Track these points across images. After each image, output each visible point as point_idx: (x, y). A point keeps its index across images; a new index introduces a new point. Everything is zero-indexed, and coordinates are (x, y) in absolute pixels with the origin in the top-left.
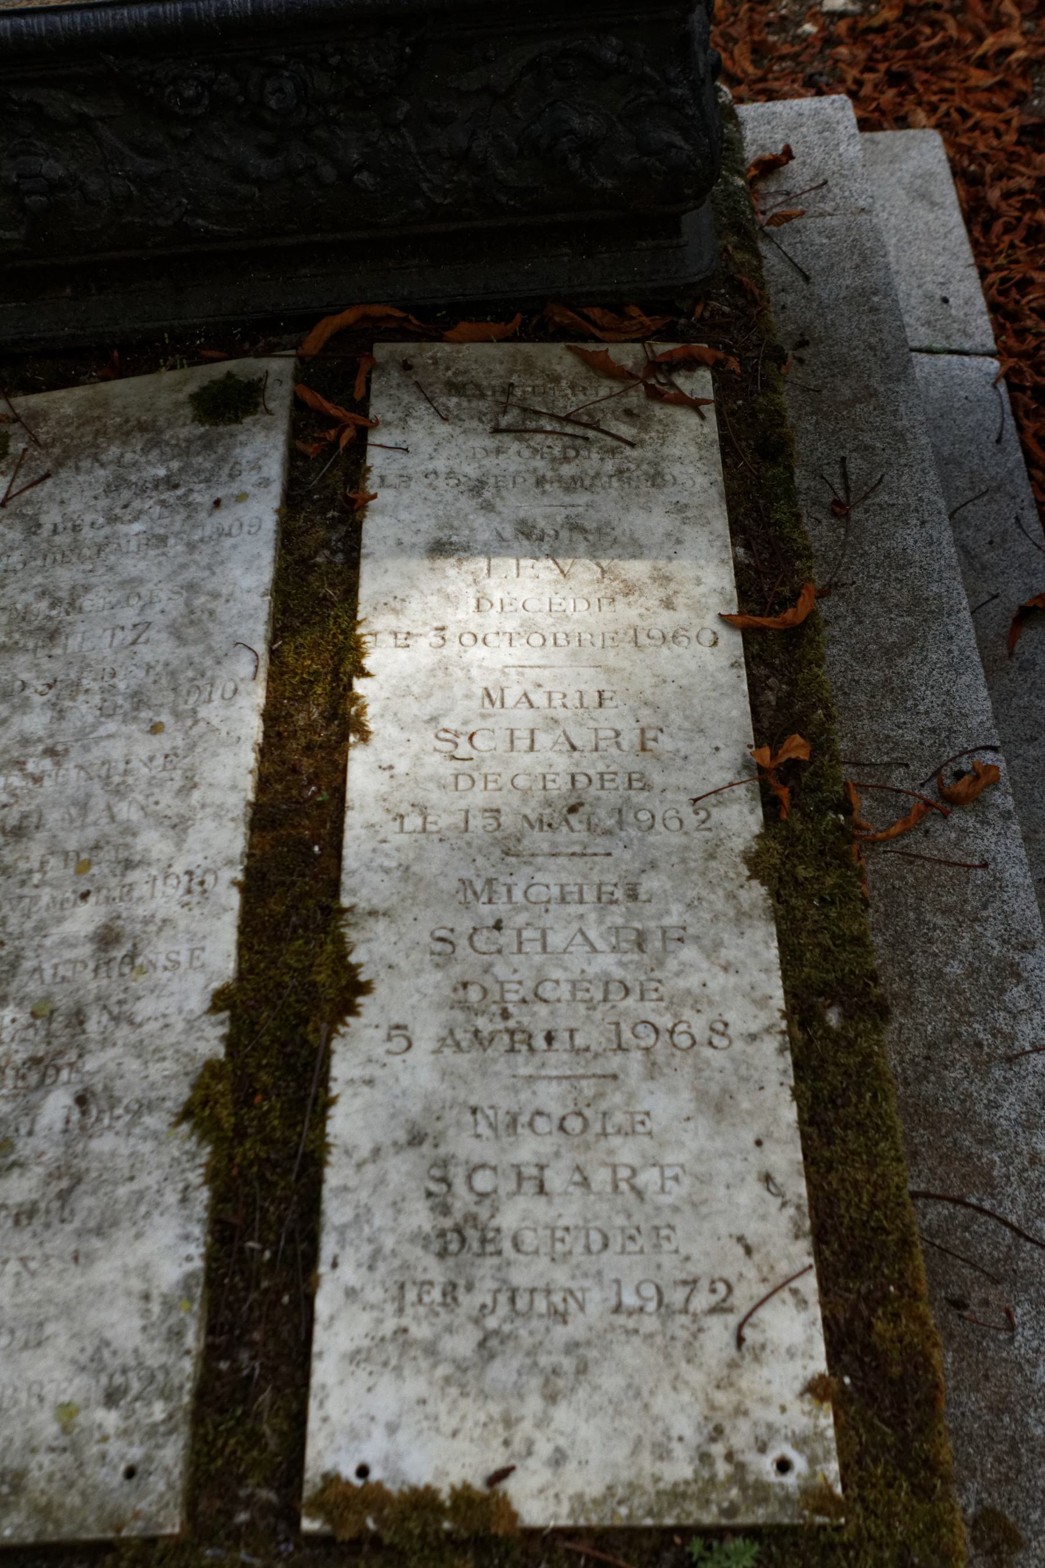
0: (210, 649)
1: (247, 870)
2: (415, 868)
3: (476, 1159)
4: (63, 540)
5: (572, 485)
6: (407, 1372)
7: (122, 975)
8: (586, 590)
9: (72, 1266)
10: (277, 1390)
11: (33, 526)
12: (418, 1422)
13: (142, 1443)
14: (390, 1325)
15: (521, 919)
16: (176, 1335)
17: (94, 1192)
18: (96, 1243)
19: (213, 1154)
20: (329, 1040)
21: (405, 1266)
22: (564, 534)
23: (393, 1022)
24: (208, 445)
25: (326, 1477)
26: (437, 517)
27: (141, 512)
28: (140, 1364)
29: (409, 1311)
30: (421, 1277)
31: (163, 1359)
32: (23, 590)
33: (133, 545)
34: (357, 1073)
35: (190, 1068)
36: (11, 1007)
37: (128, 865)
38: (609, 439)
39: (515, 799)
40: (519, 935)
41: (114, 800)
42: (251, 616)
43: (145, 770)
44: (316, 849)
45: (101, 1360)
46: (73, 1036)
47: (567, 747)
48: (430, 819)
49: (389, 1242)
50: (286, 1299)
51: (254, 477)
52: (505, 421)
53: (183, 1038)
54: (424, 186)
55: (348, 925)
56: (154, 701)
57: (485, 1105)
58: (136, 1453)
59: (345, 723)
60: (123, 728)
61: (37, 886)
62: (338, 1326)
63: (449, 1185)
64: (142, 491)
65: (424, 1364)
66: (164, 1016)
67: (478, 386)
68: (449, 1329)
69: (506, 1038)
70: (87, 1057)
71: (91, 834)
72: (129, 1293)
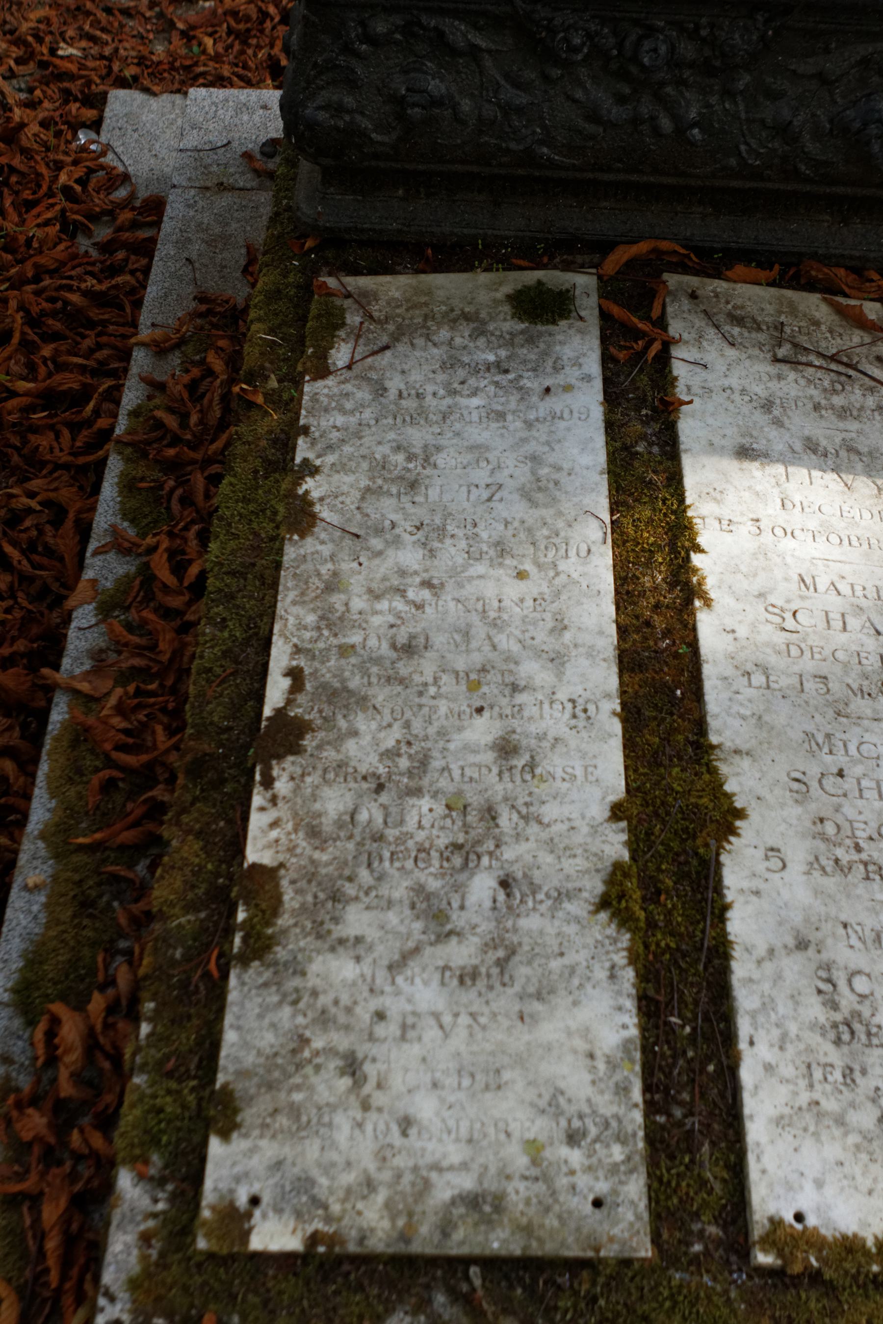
0: (560, 514)
1: (623, 705)
2: (766, 718)
3: (852, 966)
4: (409, 404)
5: (843, 413)
6: (824, 1138)
7: (524, 781)
8: (868, 503)
9: (519, 1023)
10: (713, 1144)
11: (380, 390)
12: (840, 1180)
13: (606, 1178)
14: (804, 1098)
15: (859, 770)
16: (623, 1090)
17: (529, 963)
18: (537, 1006)
19: (632, 940)
20: (718, 854)
21: (809, 1050)
22: (843, 453)
23: (769, 845)
24: (531, 340)
25: (771, 1220)
26: (738, 426)
27: (477, 389)
28: (594, 1112)
29: (818, 1087)
30: (823, 1060)
31: (614, 1109)
32: (380, 443)
33: (475, 417)
34: (745, 884)
35: (600, 866)
36: (427, 798)
37: (515, 688)
38: (867, 379)
39: (838, 669)
40: (859, 783)
41: (493, 632)
42: (593, 490)
43: (518, 610)
44: (679, 692)
45: (558, 1106)
46: (489, 829)
47: (873, 632)
48: (772, 678)
49: (793, 1028)
50: (711, 1068)
51: (577, 373)
52: (781, 352)
53: (589, 840)
54: (743, 148)
55: (719, 759)
56: (515, 552)
57: (853, 921)
58: (602, 1187)
59: (687, 591)
60: (491, 572)
61: (434, 698)
62: (762, 1094)
63: (834, 986)
64: (476, 371)
65: (837, 1132)
66: (569, 820)
67: (754, 320)
68: (853, 1105)
69: (862, 867)
70: (504, 848)
71: (477, 659)
72: (575, 1052)
